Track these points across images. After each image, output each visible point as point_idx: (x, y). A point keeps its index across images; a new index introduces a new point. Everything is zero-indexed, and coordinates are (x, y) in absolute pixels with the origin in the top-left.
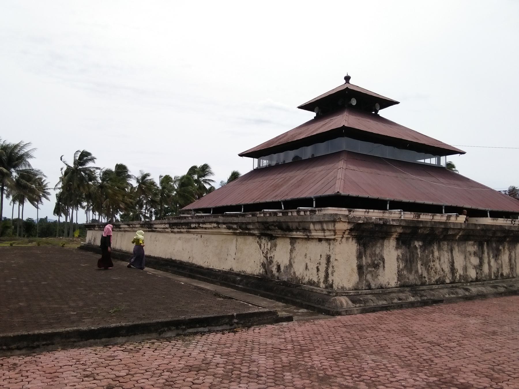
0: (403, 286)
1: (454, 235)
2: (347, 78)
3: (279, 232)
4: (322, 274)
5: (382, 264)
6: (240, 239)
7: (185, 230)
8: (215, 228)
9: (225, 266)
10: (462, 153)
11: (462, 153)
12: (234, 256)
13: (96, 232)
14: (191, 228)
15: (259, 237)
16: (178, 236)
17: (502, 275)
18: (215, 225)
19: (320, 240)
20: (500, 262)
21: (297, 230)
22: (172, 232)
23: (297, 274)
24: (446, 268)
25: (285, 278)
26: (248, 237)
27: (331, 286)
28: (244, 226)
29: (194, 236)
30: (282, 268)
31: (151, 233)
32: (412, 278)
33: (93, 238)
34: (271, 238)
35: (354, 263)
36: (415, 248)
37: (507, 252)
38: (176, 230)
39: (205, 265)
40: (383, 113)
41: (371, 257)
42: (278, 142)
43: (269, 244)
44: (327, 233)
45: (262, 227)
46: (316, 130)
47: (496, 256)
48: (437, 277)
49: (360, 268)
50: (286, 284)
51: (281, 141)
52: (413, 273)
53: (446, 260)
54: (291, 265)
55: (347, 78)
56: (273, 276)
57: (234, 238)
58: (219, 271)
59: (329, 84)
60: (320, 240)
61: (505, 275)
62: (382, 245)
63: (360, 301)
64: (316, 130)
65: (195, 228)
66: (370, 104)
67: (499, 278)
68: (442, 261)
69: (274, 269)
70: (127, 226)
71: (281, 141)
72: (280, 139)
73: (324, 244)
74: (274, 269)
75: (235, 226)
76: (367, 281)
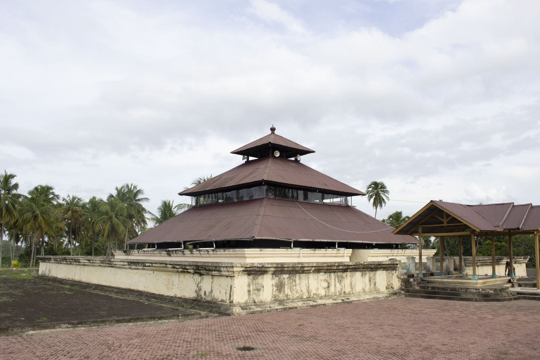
0: (276, 300)
1: (310, 270)
2: (273, 130)
3: (205, 271)
4: (228, 296)
5: (262, 289)
6: (182, 276)
7: (141, 267)
8: (163, 267)
9: (171, 294)
10: (313, 152)
11: (313, 152)
12: (177, 286)
13: (51, 264)
14: (145, 266)
15: (193, 274)
16: (135, 271)
17: (344, 292)
18: (164, 265)
19: (227, 276)
20: (343, 284)
21: (215, 271)
22: (130, 268)
23: (215, 296)
24: (304, 290)
25: (209, 299)
26: (186, 274)
27: (232, 302)
28: (184, 267)
29: (149, 272)
30: (207, 294)
31: (110, 268)
32: (281, 296)
33: (48, 270)
34: (201, 275)
35: (246, 289)
36: (284, 278)
37: (349, 278)
38: (133, 267)
39: (157, 292)
40: (303, 159)
41: (255, 285)
42: (213, 185)
43: (200, 278)
44: (230, 273)
45: (195, 268)
46: (241, 180)
47: (340, 282)
48: (298, 295)
49: (249, 291)
50: (208, 302)
51: (215, 184)
52: (282, 293)
53: (304, 285)
54: (212, 291)
55: (273, 130)
56: (202, 298)
57: (177, 274)
58: (168, 296)
59: (254, 136)
60: (227, 276)
61: (347, 292)
62: (263, 278)
63: (246, 309)
64: (241, 180)
65: (149, 266)
66: (290, 153)
67: (343, 294)
68: (301, 286)
69: (203, 294)
70: (87, 261)
71: (215, 184)
72: (216, 181)
73: (229, 278)
74: (203, 294)
75: (178, 267)
76: (253, 298)
